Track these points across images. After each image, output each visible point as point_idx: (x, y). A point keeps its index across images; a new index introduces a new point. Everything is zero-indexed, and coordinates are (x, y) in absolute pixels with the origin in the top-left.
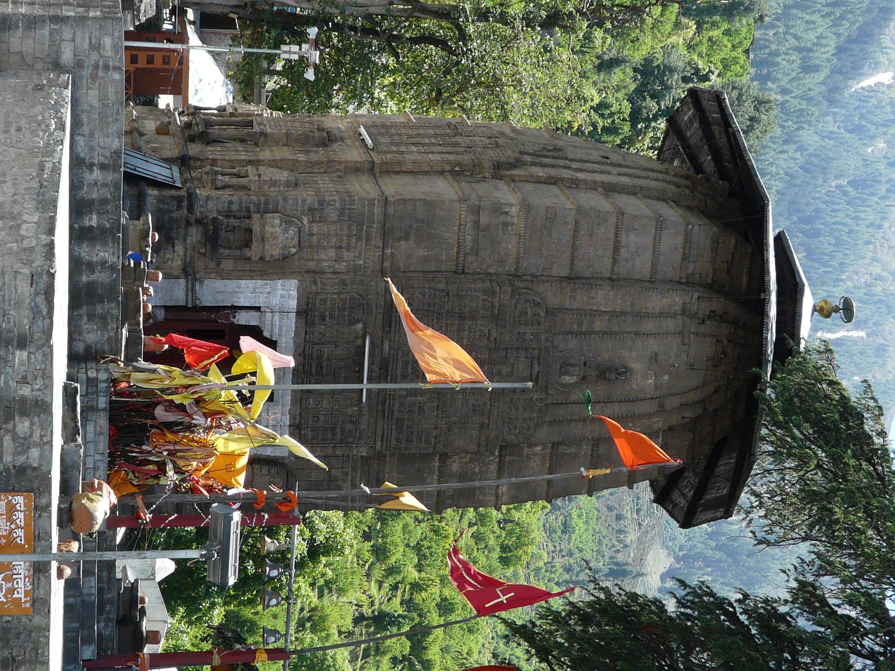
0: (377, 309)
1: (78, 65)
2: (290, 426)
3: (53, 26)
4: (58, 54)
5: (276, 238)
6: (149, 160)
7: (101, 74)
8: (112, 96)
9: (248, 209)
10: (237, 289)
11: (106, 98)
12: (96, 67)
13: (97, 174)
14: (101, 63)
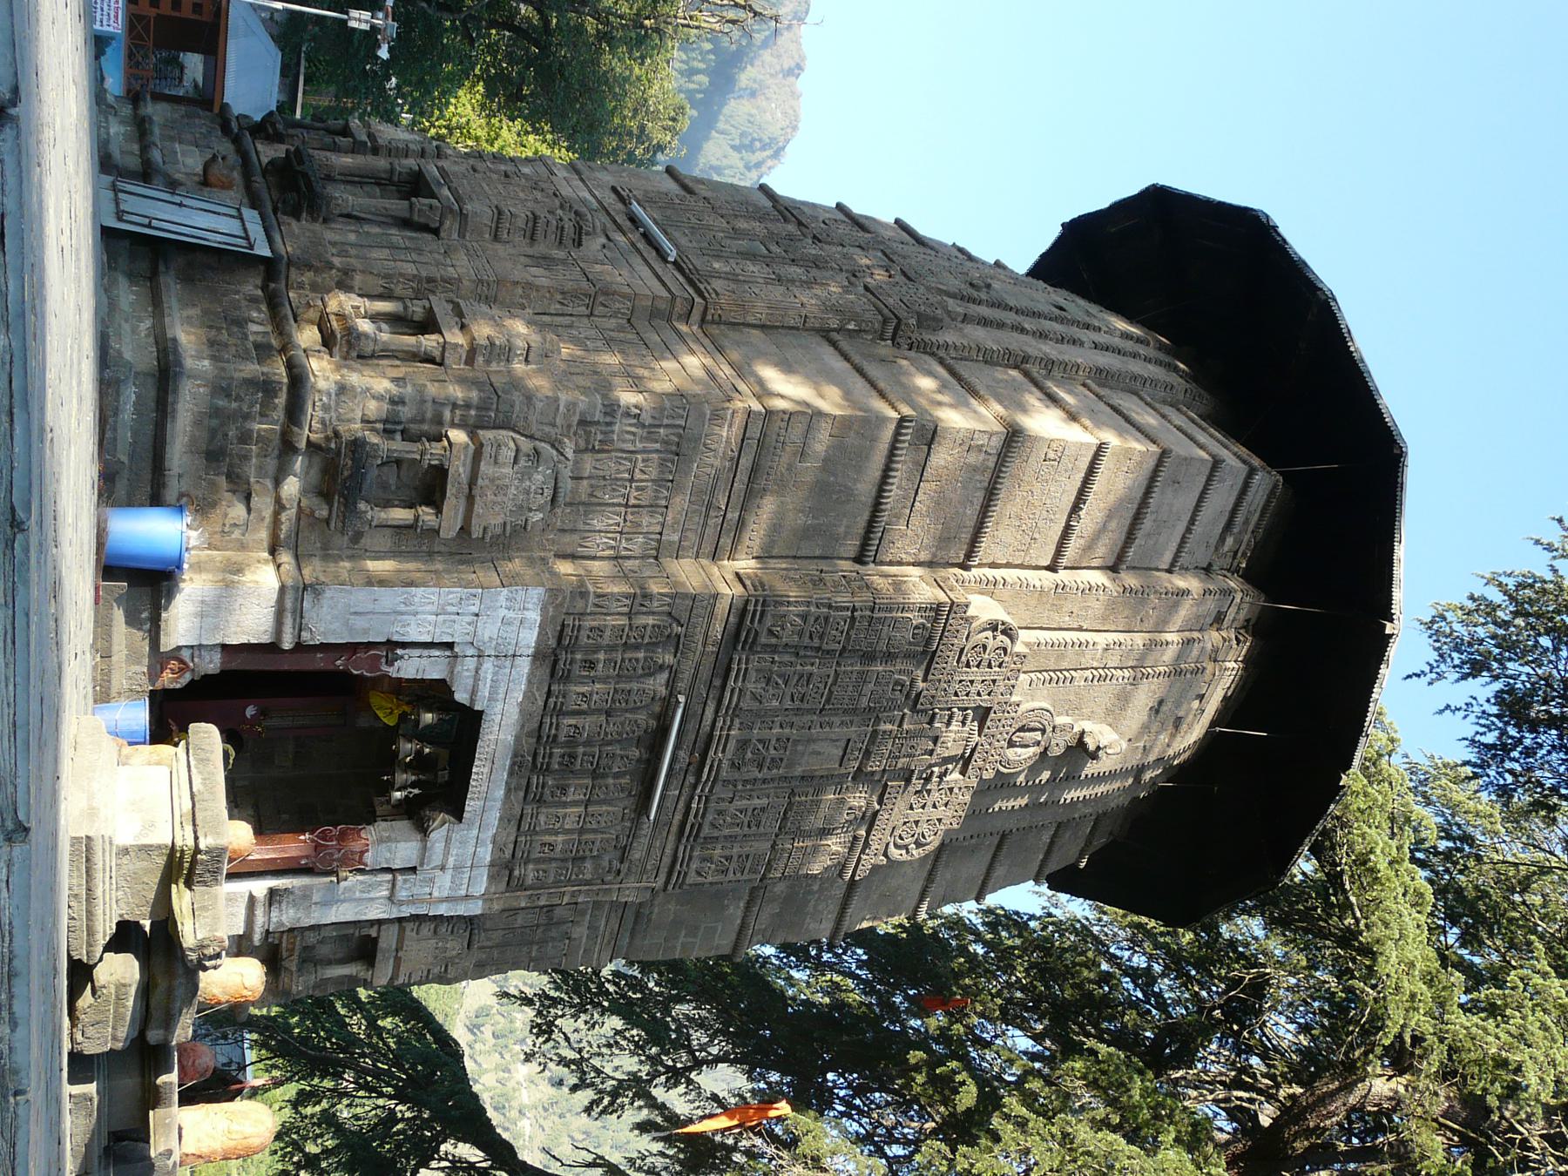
0: (705, 644)
2: (492, 865)
5: (501, 489)
6: (187, 202)
10: (402, 608)
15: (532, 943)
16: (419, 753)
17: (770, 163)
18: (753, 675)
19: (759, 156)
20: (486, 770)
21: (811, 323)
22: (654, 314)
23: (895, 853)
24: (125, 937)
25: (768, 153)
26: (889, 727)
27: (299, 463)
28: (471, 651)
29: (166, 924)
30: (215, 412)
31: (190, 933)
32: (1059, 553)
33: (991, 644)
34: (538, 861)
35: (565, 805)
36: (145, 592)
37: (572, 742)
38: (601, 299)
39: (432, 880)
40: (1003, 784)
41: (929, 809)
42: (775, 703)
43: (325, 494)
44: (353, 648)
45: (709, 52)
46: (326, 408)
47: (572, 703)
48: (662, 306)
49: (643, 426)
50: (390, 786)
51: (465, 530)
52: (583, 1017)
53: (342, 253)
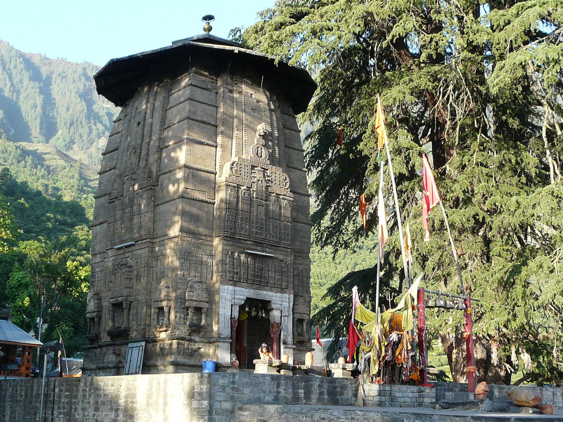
1: (233, 399)
3: (214, 414)
4: (226, 410)
6: (129, 359)
7: (236, 386)
8: (245, 380)
9: (183, 308)
11: (247, 383)
12: (233, 389)
13: (282, 390)
14: (231, 386)
15: (303, 280)
16: (255, 311)
18: (241, 232)
21: (153, 210)
23: (287, 186)
24: (279, 371)
26: (255, 194)
27: (193, 338)
29: (278, 366)
30: (183, 354)
31: (278, 364)
32: (213, 146)
33: (236, 169)
34: (282, 282)
35: (269, 276)
36: (220, 369)
37: (254, 276)
39: (284, 307)
40: (271, 157)
43: (200, 332)
44: (231, 326)
46: (182, 332)
47: (245, 276)
48: (150, 249)
50: (262, 317)
51: (207, 302)
52: (344, 231)
53: (140, 325)
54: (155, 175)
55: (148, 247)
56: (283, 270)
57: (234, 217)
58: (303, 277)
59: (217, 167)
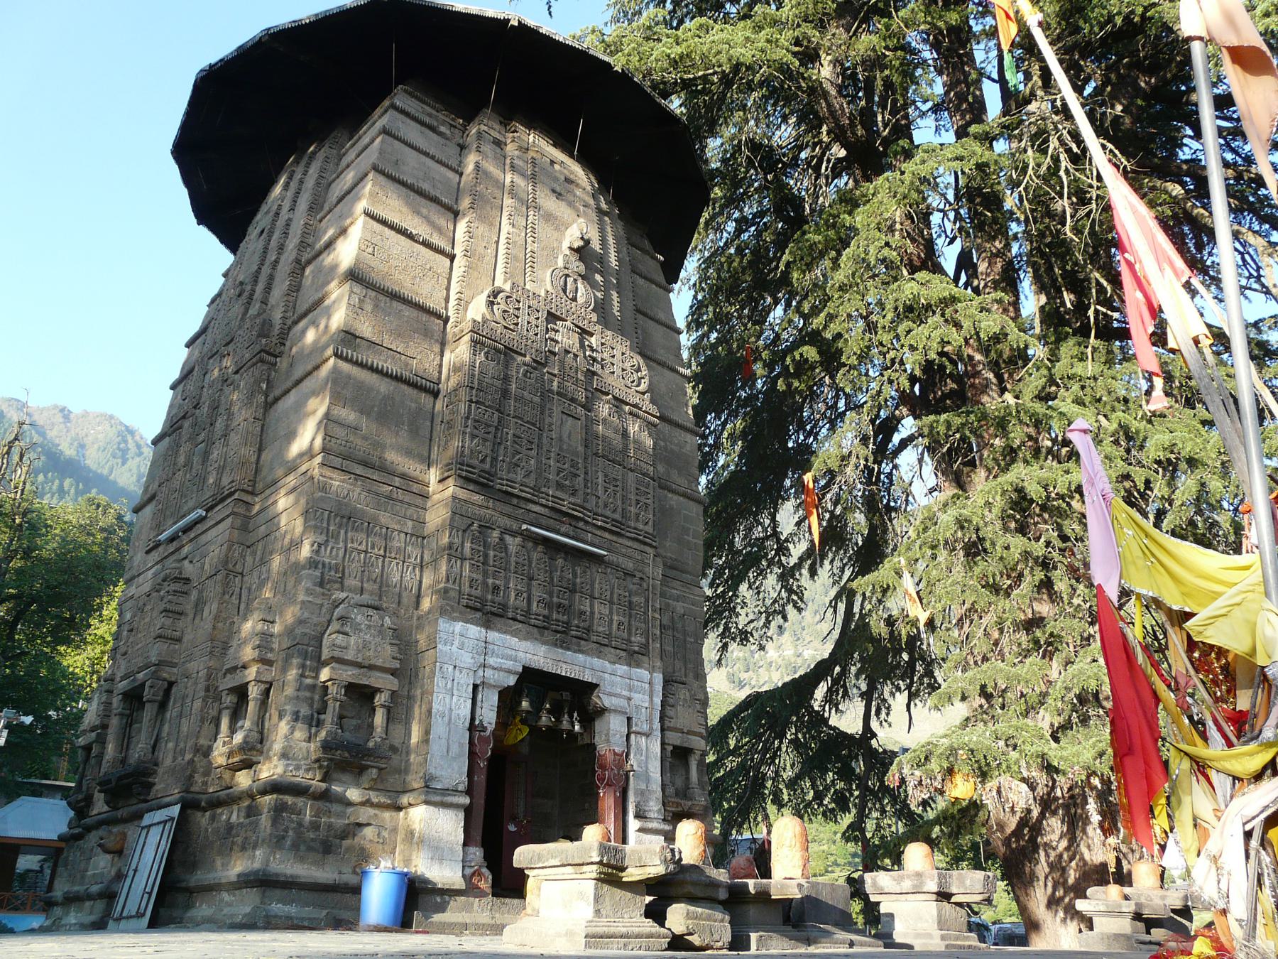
6: (133, 866)
10: (446, 719)
16: (549, 712)
17: (137, 438)
18: (511, 476)
19: (131, 445)
20: (564, 666)
21: (260, 414)
22: (245, 529)
24: (656, 913)
25: (129, 438)
26: (555, 384)
27: (336, 788)
28: (480, 673)
29: (649, 886)
31: (656, 869)
33: (503, 307)
35: (592, 613)
36: (422, 899)
37: (549, 606)
38: (230, 566)
39: (637, 707)
40: (601, 308)
41: (614, 361)
42: (533, 462)
43: (361, 770)
44: (472, 755)
45: (46, 477)
46: (298, 768)
48: (238, 522)
49: (327, 541)
51: (394, 673)
54: (276, 331)
55: (233, 513)
56: (634, 599)
57: (492, 430)
58: (685, 633)
59: (452, 303)
